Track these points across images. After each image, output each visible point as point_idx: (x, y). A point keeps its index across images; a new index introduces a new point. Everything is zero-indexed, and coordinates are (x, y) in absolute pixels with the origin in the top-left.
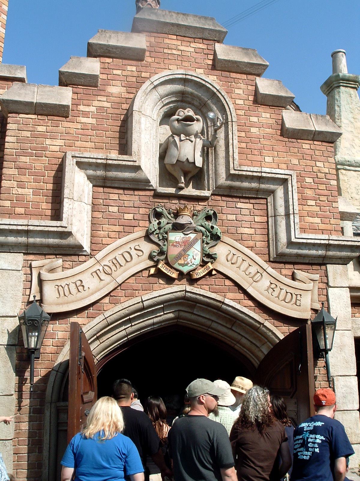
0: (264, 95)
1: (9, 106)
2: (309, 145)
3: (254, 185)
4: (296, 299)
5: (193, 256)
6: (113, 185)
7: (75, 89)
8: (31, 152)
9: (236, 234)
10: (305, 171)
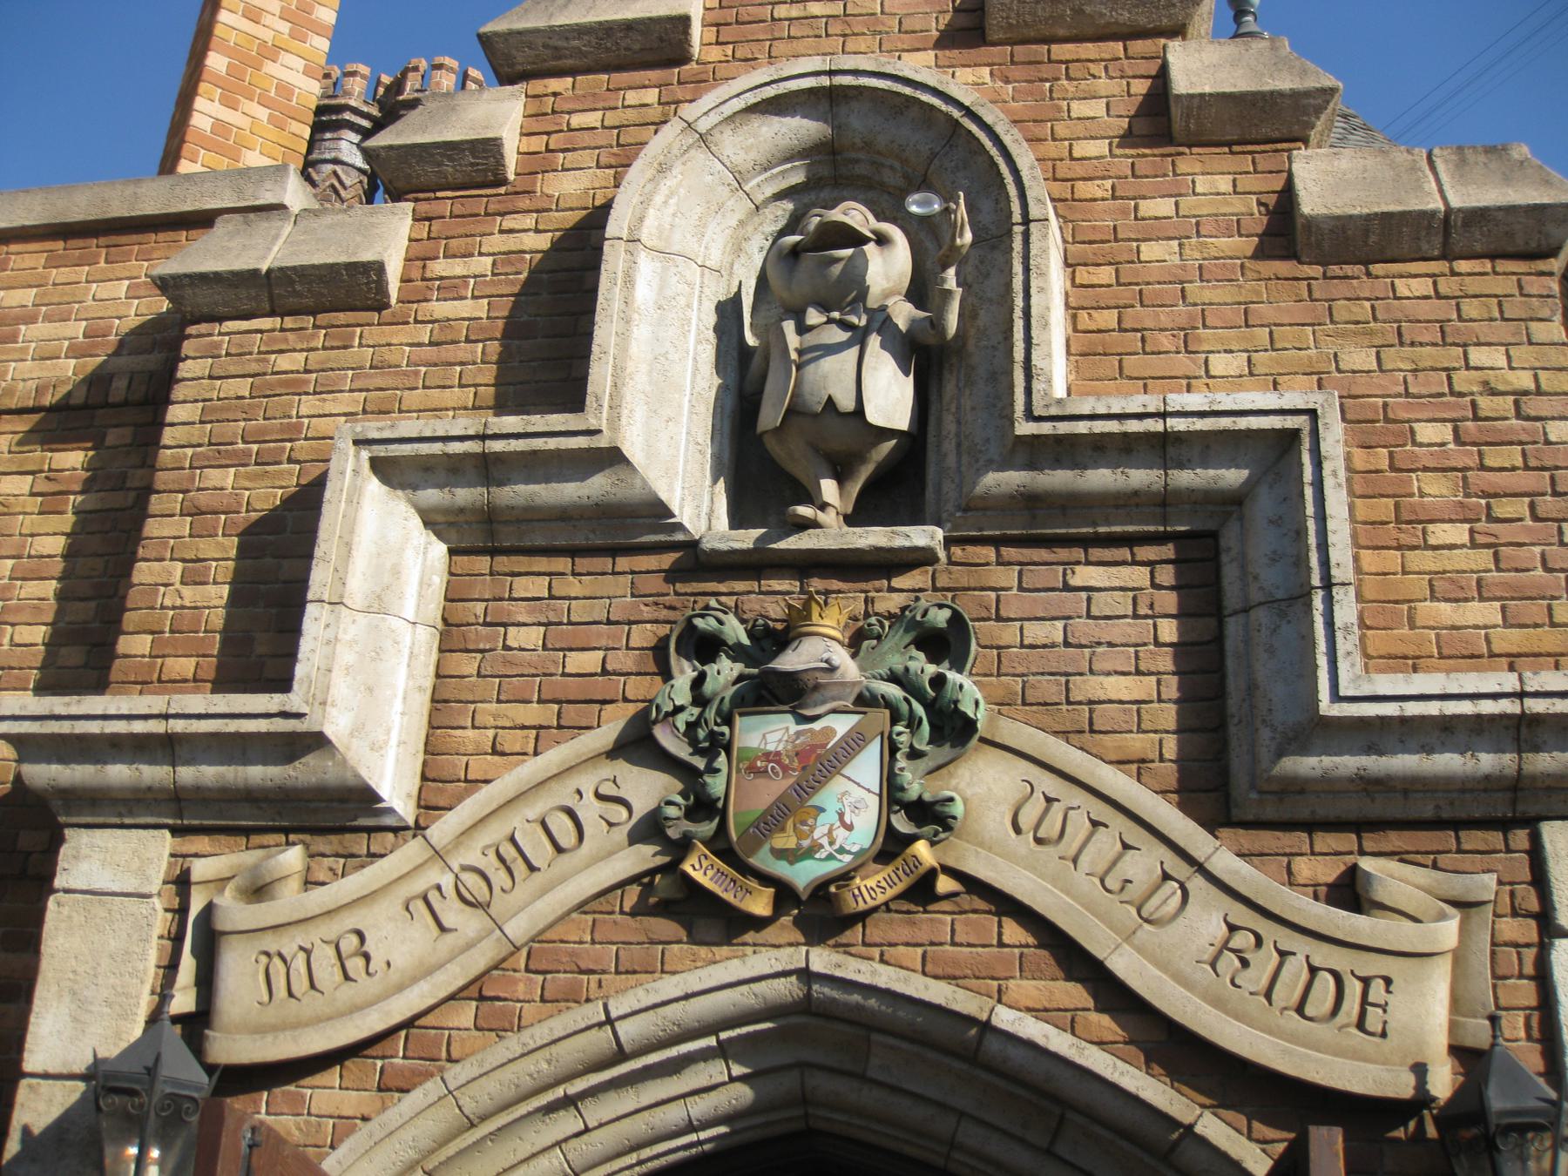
0: (1196, 102)
1: (183, 297)
2: (1430, 281)
3: (1141, 477)
4: (1364, 1001)
5: (841, 815)
6: (527, 543)
7: (424, 207)
8: (243, 451)
9: (1064, 707)
10: (1414, 397)
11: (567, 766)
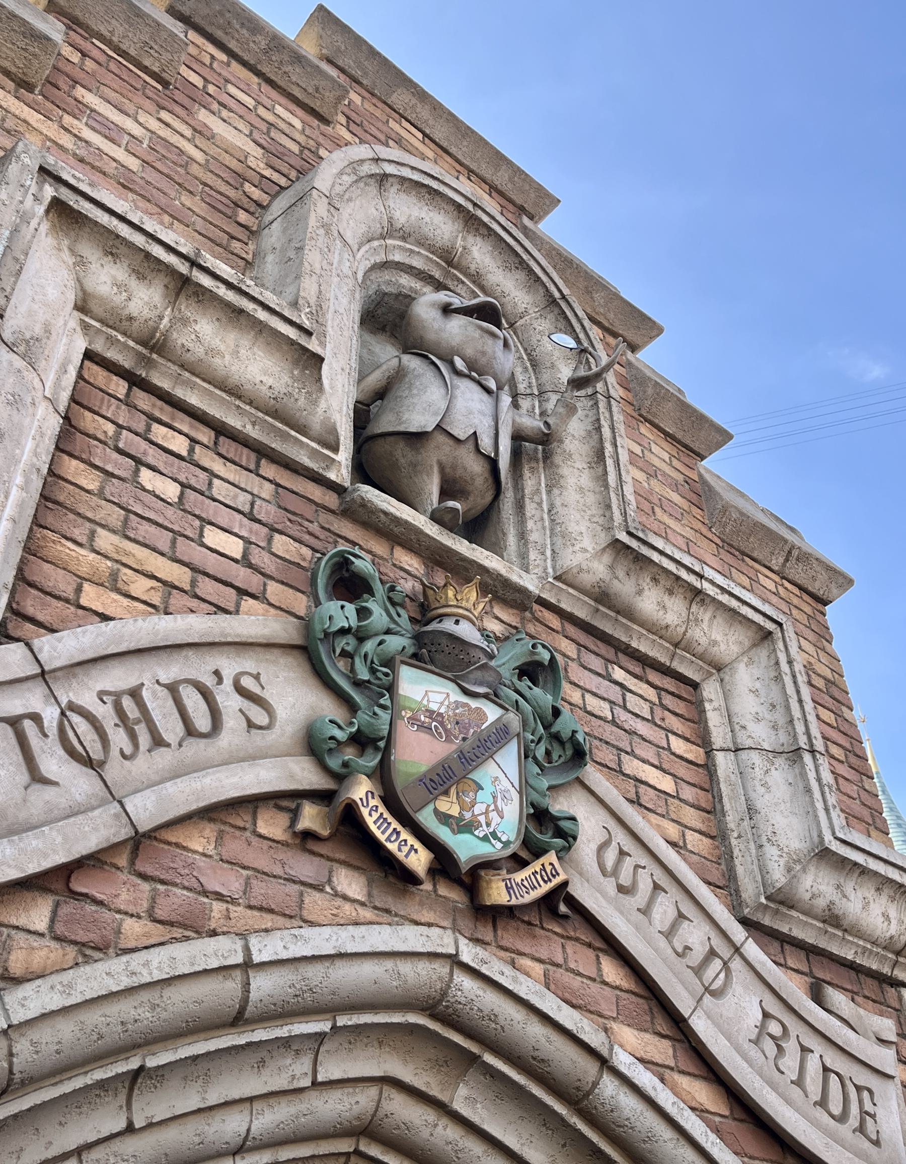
11: (210, 640)
